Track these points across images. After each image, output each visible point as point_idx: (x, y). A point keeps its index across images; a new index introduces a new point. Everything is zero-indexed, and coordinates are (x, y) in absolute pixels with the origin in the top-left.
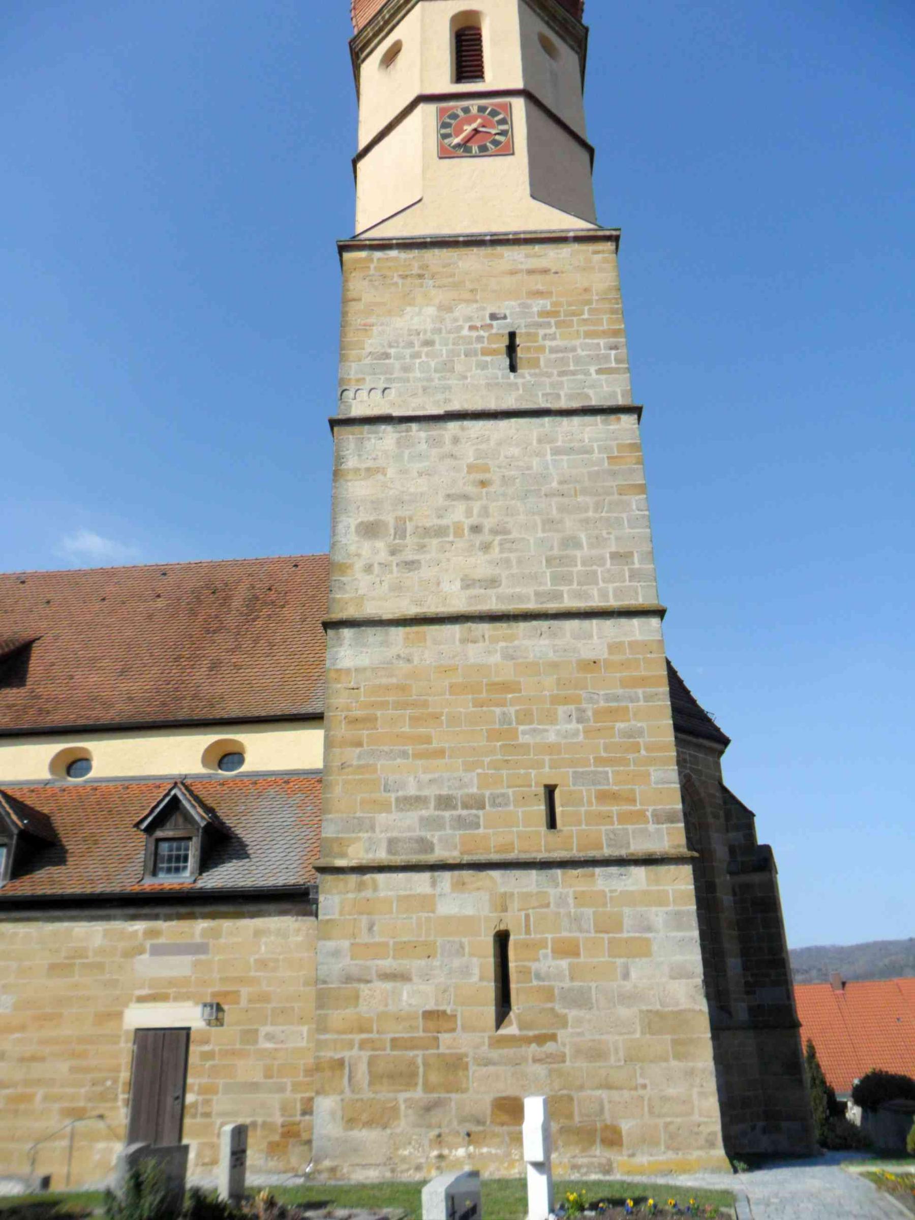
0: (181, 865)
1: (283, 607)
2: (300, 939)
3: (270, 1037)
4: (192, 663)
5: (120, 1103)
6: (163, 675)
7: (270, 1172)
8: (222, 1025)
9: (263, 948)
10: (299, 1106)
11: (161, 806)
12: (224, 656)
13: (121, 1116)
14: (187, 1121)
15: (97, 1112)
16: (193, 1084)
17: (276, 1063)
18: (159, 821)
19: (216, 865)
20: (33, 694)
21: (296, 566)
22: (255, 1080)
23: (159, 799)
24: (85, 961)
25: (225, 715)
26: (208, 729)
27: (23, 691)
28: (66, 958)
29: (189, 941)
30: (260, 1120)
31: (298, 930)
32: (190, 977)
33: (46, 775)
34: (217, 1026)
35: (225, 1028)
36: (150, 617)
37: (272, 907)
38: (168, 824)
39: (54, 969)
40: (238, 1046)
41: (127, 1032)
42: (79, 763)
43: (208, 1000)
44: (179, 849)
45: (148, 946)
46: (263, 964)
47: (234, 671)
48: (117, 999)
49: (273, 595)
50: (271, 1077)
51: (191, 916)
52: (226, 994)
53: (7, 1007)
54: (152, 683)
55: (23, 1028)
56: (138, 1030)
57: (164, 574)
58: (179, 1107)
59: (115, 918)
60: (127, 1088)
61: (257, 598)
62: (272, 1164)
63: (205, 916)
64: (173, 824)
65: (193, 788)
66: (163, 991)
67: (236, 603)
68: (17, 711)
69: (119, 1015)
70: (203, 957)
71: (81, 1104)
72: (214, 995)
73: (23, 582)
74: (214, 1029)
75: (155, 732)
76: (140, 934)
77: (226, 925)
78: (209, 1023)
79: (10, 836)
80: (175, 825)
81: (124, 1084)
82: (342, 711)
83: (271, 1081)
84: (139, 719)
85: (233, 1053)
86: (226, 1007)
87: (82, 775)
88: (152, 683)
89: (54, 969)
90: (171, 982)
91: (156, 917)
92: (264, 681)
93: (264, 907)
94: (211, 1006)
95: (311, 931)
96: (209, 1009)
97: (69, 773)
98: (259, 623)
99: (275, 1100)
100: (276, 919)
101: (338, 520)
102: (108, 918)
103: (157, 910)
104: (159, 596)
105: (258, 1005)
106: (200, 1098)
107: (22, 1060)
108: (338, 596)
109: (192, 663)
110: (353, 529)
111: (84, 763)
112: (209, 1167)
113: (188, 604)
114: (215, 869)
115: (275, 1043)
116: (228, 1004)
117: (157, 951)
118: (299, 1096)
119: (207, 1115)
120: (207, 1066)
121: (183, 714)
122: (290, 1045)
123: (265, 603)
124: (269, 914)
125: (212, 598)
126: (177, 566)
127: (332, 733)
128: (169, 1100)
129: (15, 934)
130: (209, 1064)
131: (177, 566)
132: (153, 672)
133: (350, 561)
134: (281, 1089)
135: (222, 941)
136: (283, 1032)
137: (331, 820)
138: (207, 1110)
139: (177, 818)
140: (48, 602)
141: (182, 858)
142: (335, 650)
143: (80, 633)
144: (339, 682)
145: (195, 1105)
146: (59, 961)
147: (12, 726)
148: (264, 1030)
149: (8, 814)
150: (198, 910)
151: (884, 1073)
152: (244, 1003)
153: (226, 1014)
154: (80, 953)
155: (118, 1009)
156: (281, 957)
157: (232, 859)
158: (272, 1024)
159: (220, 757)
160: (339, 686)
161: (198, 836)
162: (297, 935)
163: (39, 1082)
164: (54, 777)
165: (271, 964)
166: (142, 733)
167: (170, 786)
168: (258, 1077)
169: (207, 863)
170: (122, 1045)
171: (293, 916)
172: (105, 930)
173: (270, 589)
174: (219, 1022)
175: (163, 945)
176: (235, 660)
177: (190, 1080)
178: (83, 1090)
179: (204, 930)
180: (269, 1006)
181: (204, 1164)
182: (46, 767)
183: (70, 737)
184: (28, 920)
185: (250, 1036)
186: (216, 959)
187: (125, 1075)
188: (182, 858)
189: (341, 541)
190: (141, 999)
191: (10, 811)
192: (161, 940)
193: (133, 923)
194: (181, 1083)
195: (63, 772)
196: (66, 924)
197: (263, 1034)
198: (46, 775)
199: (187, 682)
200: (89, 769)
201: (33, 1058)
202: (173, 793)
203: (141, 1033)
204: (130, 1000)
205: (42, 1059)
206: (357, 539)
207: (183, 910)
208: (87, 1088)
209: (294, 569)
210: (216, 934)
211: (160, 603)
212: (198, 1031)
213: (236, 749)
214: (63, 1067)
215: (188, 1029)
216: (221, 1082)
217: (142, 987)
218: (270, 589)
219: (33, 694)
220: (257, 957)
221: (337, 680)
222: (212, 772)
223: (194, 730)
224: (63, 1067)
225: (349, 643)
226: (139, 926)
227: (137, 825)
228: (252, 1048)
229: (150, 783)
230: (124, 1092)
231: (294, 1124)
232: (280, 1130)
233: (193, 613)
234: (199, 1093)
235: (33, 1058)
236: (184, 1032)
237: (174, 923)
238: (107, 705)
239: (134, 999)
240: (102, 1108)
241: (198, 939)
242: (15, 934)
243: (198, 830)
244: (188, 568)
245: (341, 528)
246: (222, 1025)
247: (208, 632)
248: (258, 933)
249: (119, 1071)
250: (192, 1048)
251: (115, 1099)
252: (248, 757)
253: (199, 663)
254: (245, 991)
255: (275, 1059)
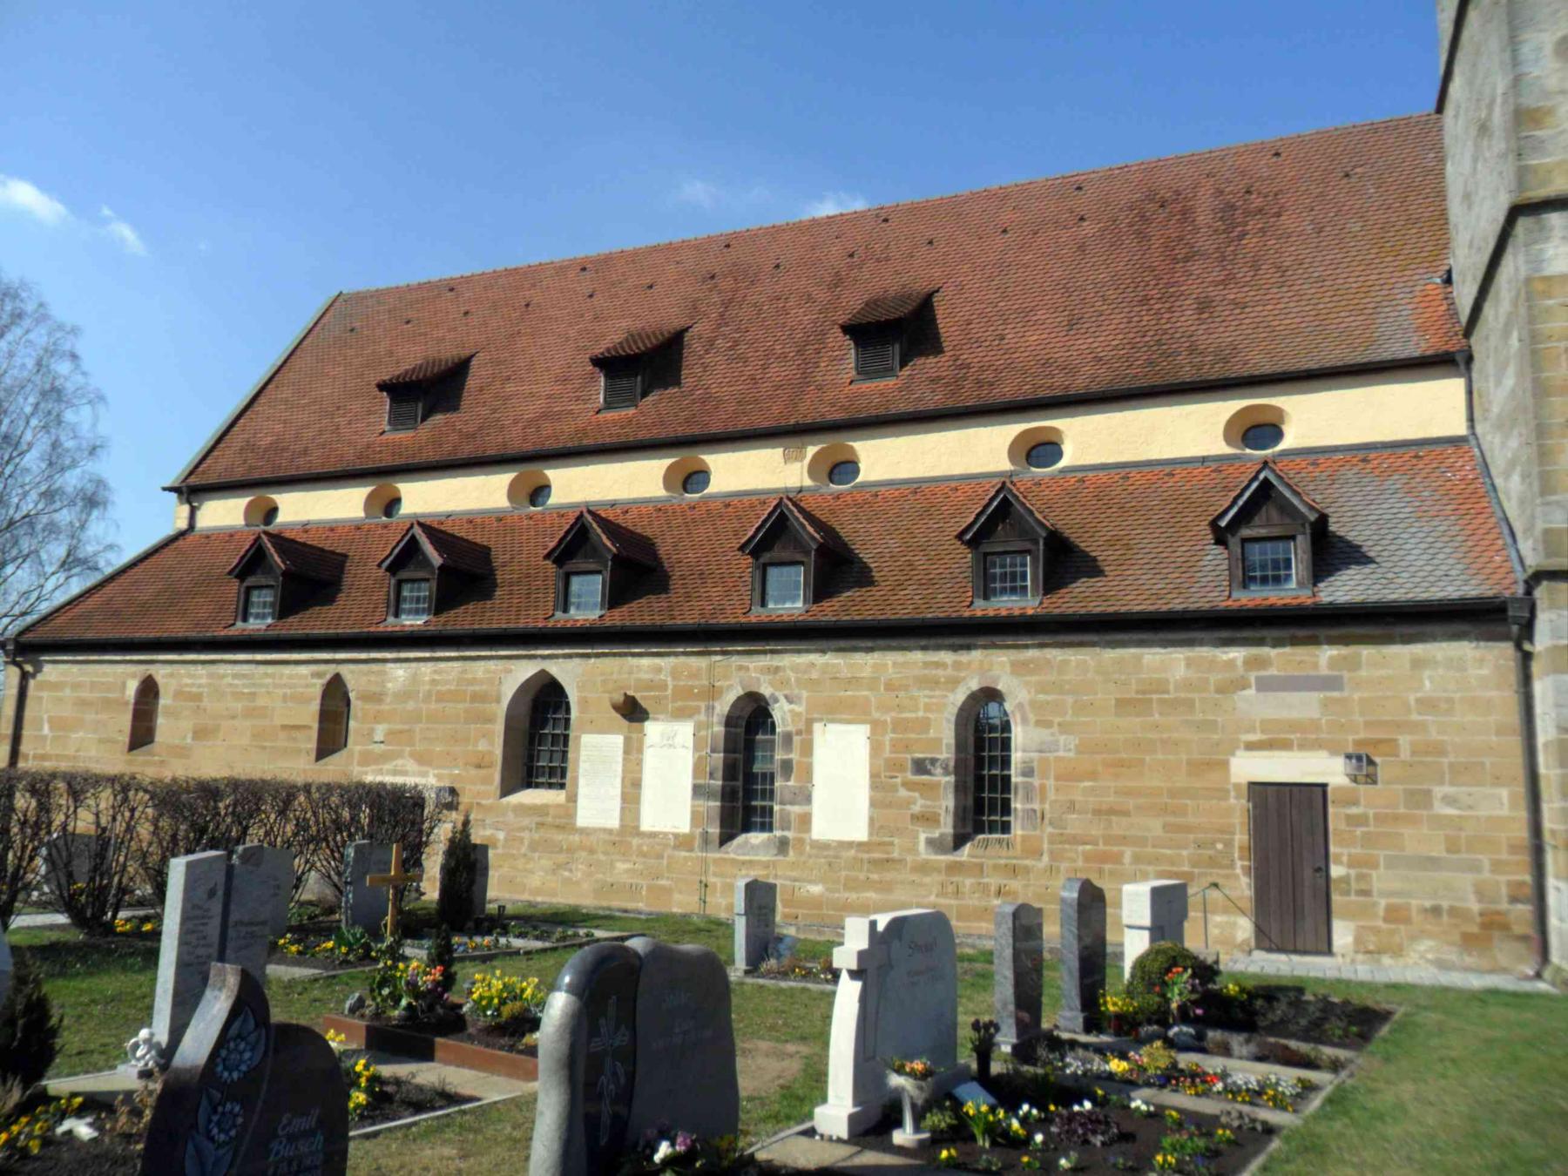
0: (1282, 573)
1: (1278, 215)
2: (1485, 672)
3: (1449, 801)
4: (1167, 305)
5: (1238, 871)
6: (1132, 325)
7: (1467, 969)
8: (1375, 782)
9: (1427, 683)
10: (1504, 891)
11: (1247, 494)
12: (1213, 292)
13: (1243, 887)
14: (1336, 898)
15: (1211, 880)
16: (1339, 856)
17: (1463, 834)
18: (1247, 514)
19: (1330, 574)
20: (959, 362)
21: (1277, 154)
22: (1434, 854)
23: (1244, 485)
24: (1166, 696)
25: (1246, 371)
26: (1229, 393)
27: (943, 359)
28: (1137, 692)
29: (1312, 673)
30: (1445, 904)
31: (1482, 661)
32: (1320, 719)
33: (1005, 465)
34: (1366, 783)
35: (1380, 786)
36: (1082, 248)
37: (1437, 629)
38: (1256, 518)
39: (1123, 705)
40: (1402, 810)
41: (1237, 786)
42: (695, 477)
43: (1350, 750)
44: (1013, 565)
45: (1252, 677)
46: (1427, 704)
47: (1238, 311)
48: (1218, 745)
49: (1256, 201)
50: (1458, 851)
51: (1314, 641)
52: (1377, 743)
53: (1070, 750)
54: (1121, 336)
55: (1093, 776)
56: (1252, 785)
57: (1079, 188)
58: (1322, 882)
59: (1201, 643)
60: (1247, 854)
61: (1233, 207)
62: (1469, 960)
63: (1332, 641)
64: (1264, 518)
65: (802, 504)
66: (1282, 736)
67: (1204, 217)
68: (947, 385)
69: (1225, 765)
70: (1336, 694)
71: (1186, 869)
72: (1358, 743)
73: (886, 220)
74: (1362, 788)
75: (602, 458)
76: (1239, 663)
77: (1367, 652)
78: (1355, 779)
79: (808, 553)
80: (1268, 519)
81: (1241, 848)
82: (1559, 340)
83: (1455, 856)
84: (1125, 385)
85: (1396, 818)
86: (1377, 760)
87: (1049, 466)
88: (1121, 336)
89: (1123, 705)
90: (1294, 726)
91: (1260, 642)
92: (1289, 321)
93: (1428, 629)
94: (1359, 758)
95: (1502, 662)
96: (1354, 761)
97: (686, 490)
98: (1251, 241)
99: (1465, 882)
100: (1444, 645)
101: (1521, 38)
102: (1190, 643)
103: (1265, 633)
104: (1082, 219)
105: (1429, 759)
106: (1353, 872)
107: (1097, 812)
108: (1534, 162)
109: (1167, 305)
110: (1549, 49)
111: (701, 475)
112: (1376, 956)
113: (1131, 225)
114: (1332, 579)
115: (1460, 808)
116: (1379, 756)
117: (1265, 685)
118: (1503, 878)
119: (1366, 893)
120: (1358, 833)
121: (1187, 374)
122: (1482, 813)
123: (1247, 213)
124: (1433, 638)
125: (1163, 215)
126: (1093, 176)
127: (1544, 375)
128: (1308, 873)
129: (1066, 662)
130: (1359, 831)
131: (1093, 176)
132: (1115, 321)
133: (1549, 104)
134: (1475, 867)
135: (1363, 673)
136: (1470, 795)
137: (1558, 503)
138: (1363, 886)
139: (1269, 512)
140: (931, 243)
141: (1282, 565)
142: (1538, 247)
143: (991, 278)
144: (1550, 298)
145: (1345, 879)
146: (1128, 696)
147: (950, 403)
148: (1439, 791)
149: (803, 527)
150: (1322, 632)
151: (192, 783)
152: (1405, 754)
153: (1379, 769)
154: (1161, 686)
155: (1221, 757)
156: (1458, 695)
157: (1350, 564)
158: (1452, 784)
159: (1029, 446)
160: (1551, 302)
161: (1304, 533)
162: (1480, 668)
163: (1124, 840)
164: (1018, 468)
165: (1444, 706)
166: (1134, 403)
167: (1257, 467)
168: (1438, 851)
169: (1053, 582)
170: (1232, 801)
171: (1470, 641)
172: (1188, 659)
173: (1248, 192)
174: (1372, 779)
175: (1272, 677)
176: (1232, 297)
177: (1333, 849)
178: (1185, 853)
179: (1331, 658)
180: (1445, 760)
181: (1368, 952)
182: (1005, 455)
183: (1034, 414)
184: (1081, 644)
185: (1421, 799)
186: (1356, 696)
187: (1241, 838)
188: (1282, 565)
189: (1527, 74)
190: (1250, 747)
191: (806, 523)
192: (1273, 671)
193: (1226, 649)
194: (1323, 851)
195: (825, 476)
196: (1133, 651)
197: (1439, 795)
198: (1005, 465)
199: (1171, 331)
200: (706, 482)
201: (1112, 811)
202: (1262, 476)
203: (1257, 787)
204: (1238, 748)
205: (1126, 813)
206: (1557, 66)
207: (1301, 633)
208: (1191, 850)
209: (1275, 159)
210: (1355, 665)
211: (1088, 228)
212: (1339, 789)
213: (1054, 439)
214: (1155, 826)
215: (1324, 786)
216: (1381, 854)
217: (1251, 730)
218: (1248, 192)
219: (959, 362)
220: (1419, 695)
221: (1548, 295)
222: (1238, 451)
223: (1431, 371)
224: (1155, 826)
225: (1560, 235)
226: (1237, 654)
227: (960, 536)
228: (1425, 813)
229: (754, 498)
230: (1241, 858)
231: (1498, 913)
232: (1478, 920)
233: (1142, 236)
234: (1350, 865)
235: (1112, 811)
236: (1320, 789)
237: (1288, 650)
238: (1070, 370)
239: (1242, 745)
240: (1215, 875)
241: (1324, 671)
242: (1066, 662)
243: (1303, 525)
244: (1109, 176)
245: (1526, 50)
246: (1375, 782)
247: (1175, 260)
248: (1417, 664)
249: (1233, 833)
250: (1331, 810)
251: (1232, 866)
252: (1067, 448)
253: (1178, 303)
254: (1404, 741)
255: (1461, 829)
